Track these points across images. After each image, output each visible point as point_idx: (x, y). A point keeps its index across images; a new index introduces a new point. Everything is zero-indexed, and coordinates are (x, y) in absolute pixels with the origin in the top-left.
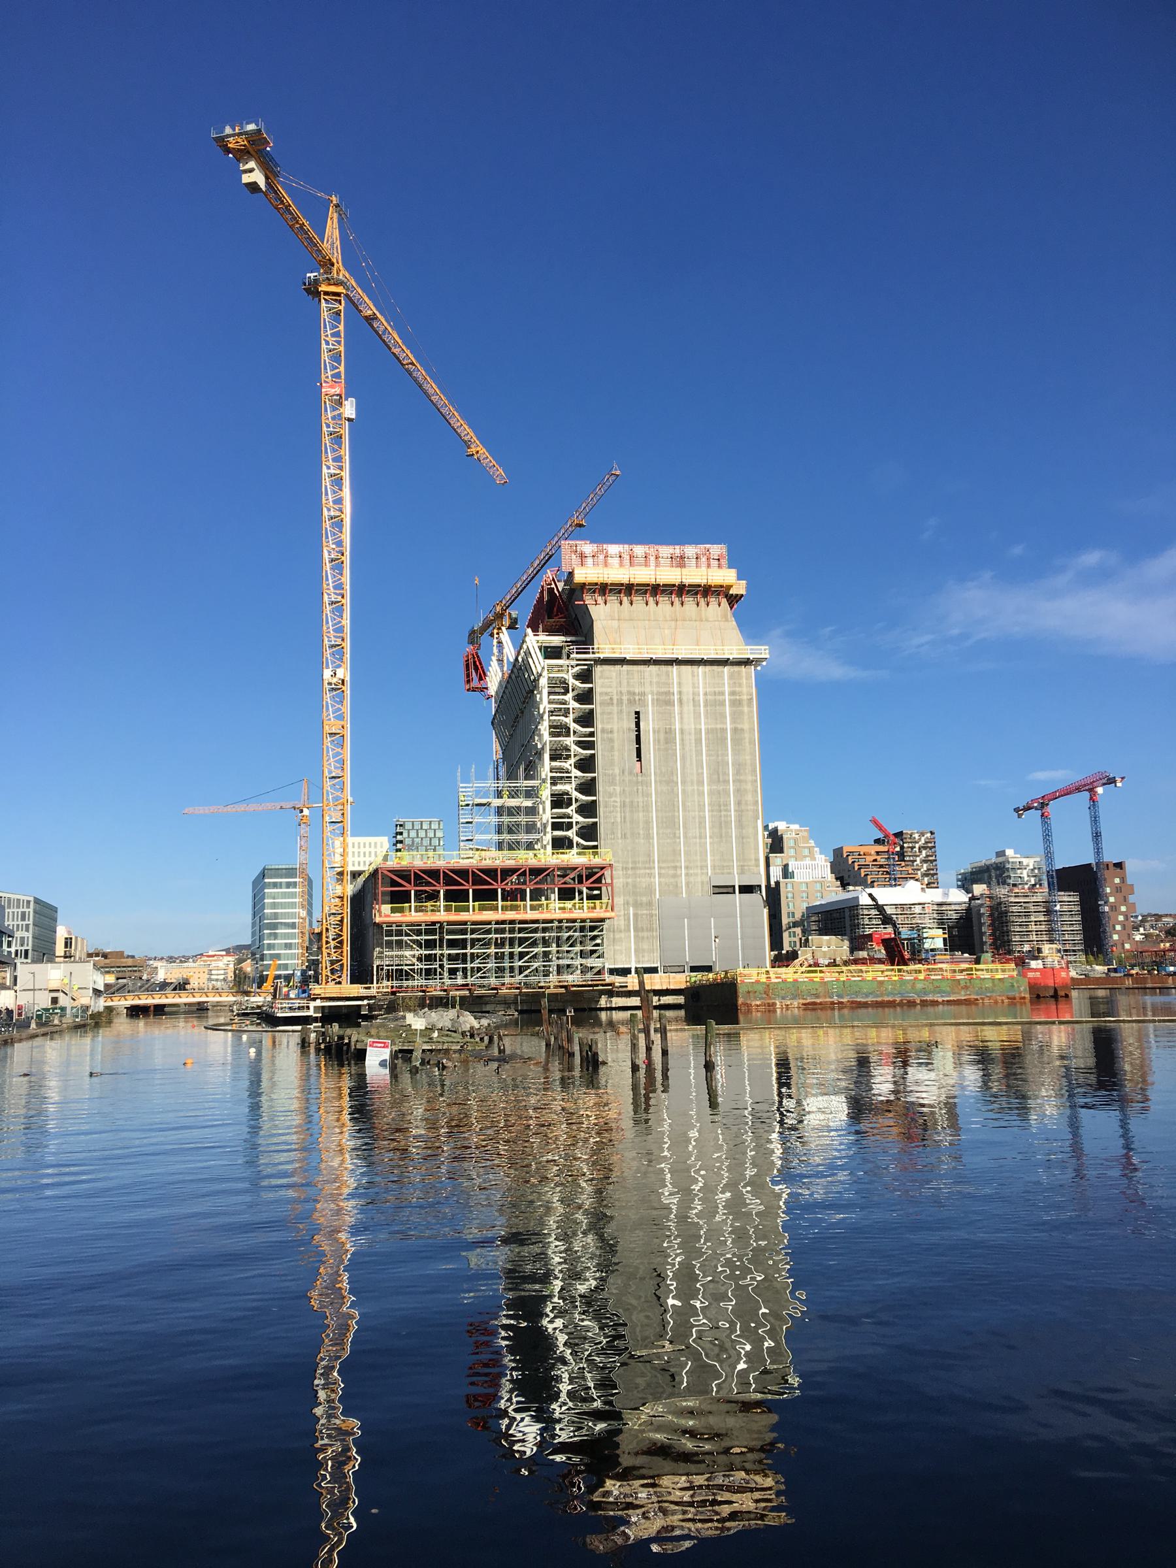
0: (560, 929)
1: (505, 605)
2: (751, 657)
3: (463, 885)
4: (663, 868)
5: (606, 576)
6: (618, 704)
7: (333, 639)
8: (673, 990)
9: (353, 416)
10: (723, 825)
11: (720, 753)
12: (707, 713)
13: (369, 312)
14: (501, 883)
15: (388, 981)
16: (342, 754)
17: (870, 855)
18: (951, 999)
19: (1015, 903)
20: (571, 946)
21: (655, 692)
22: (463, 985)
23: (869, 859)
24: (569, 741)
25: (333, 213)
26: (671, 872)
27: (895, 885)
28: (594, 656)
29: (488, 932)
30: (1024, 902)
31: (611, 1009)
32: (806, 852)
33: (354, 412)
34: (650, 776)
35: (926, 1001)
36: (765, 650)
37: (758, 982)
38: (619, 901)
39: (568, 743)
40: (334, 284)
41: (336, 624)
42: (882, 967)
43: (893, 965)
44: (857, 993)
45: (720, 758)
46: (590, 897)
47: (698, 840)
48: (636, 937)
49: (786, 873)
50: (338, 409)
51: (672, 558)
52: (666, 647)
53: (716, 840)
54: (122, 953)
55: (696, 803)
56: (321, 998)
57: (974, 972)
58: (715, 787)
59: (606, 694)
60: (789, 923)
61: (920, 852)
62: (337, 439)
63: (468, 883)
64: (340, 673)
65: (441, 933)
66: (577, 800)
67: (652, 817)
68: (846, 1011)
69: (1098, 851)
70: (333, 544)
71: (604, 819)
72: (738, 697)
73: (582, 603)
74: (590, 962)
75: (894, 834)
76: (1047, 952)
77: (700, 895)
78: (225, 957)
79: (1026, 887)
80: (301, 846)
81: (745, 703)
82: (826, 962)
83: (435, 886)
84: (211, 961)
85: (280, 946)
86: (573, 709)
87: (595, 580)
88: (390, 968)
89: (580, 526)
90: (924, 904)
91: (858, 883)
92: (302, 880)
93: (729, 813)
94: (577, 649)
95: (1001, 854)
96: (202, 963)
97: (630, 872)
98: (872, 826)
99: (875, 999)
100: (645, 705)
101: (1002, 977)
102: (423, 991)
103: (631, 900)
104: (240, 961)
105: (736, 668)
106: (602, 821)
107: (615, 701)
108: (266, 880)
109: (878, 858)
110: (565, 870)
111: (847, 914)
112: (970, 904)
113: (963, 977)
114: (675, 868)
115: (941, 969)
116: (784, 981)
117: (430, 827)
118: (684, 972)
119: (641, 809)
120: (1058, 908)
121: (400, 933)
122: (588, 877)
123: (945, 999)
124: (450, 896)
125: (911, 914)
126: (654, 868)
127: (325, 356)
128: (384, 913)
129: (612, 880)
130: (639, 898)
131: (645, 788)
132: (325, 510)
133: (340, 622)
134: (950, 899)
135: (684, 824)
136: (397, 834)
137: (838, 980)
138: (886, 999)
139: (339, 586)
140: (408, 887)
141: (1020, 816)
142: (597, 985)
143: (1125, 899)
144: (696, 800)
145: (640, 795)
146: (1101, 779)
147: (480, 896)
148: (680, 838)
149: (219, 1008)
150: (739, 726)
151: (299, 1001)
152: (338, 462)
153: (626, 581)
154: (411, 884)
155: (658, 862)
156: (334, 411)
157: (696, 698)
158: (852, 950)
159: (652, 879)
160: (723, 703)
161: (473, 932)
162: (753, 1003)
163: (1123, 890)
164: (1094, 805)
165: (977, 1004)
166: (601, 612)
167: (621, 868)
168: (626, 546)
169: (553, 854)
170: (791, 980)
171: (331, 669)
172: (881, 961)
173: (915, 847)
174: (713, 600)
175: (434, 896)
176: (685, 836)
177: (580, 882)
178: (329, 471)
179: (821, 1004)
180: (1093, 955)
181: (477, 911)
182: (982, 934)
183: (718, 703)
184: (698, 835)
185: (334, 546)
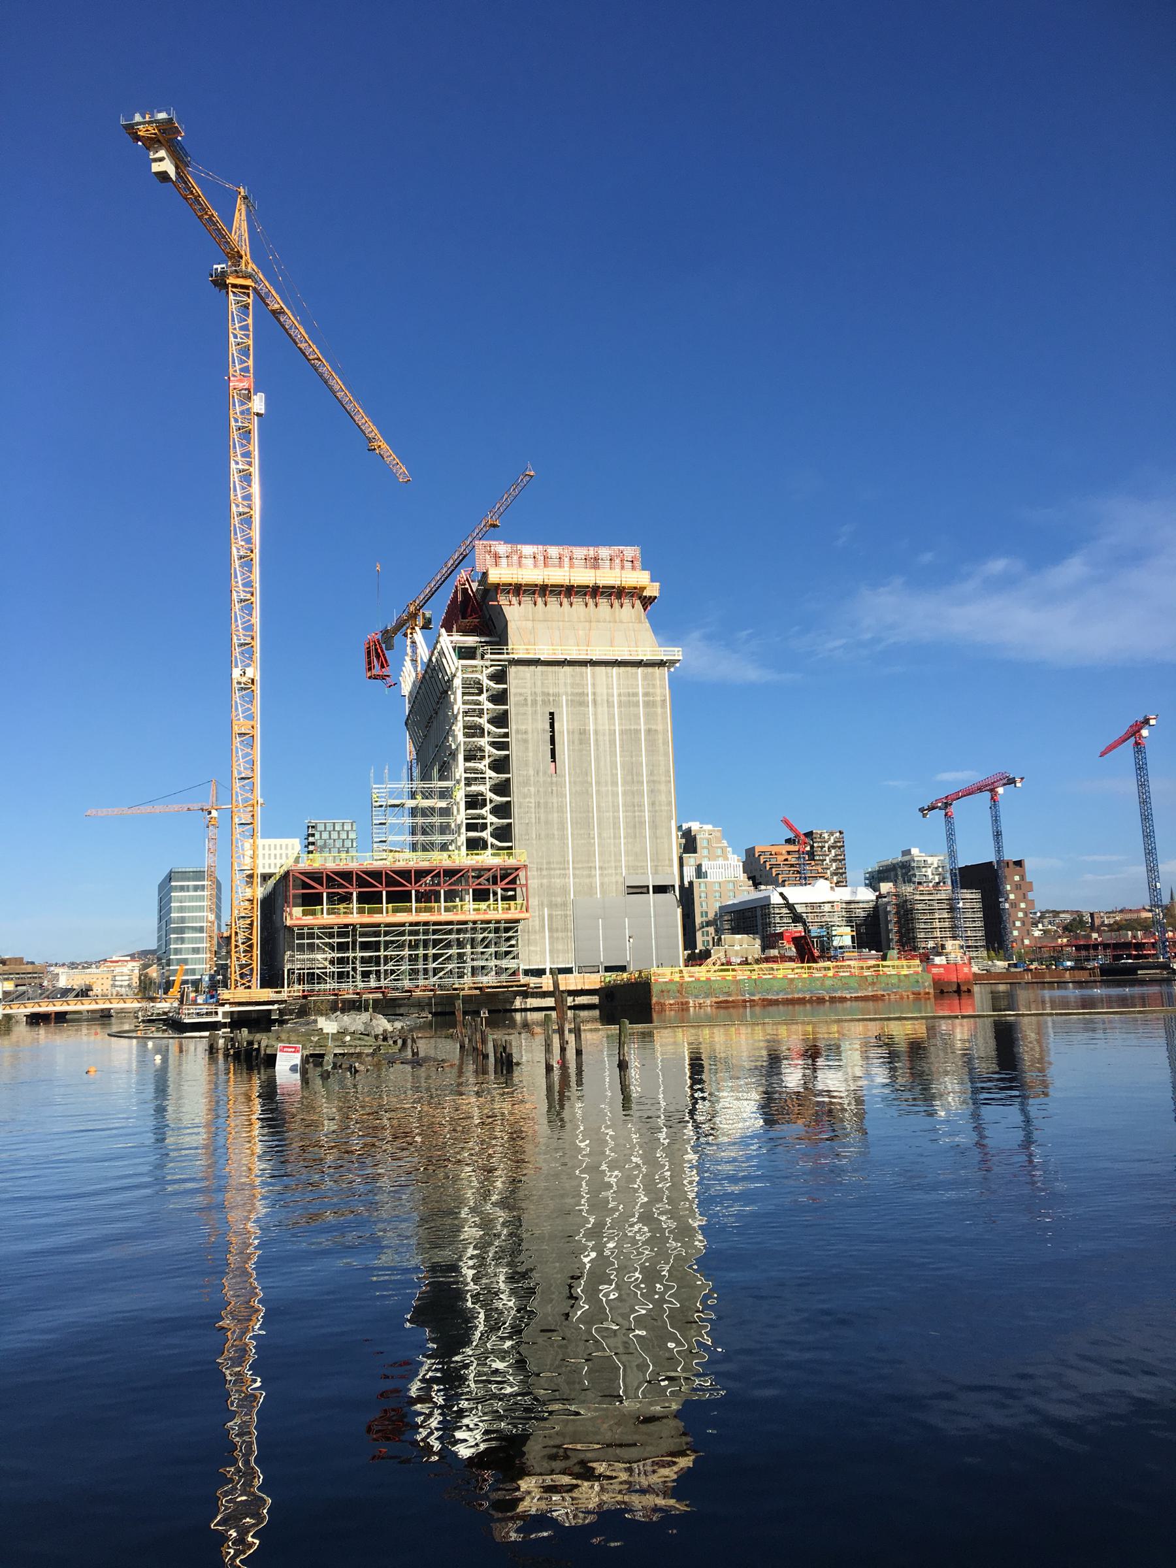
0: (474, 930)
1: (418, 605)
2: (665, 658)
3: (377, 887)
4: (579, 869)
5: (520, 576)
6: (532, 704)
7: (242, 637)
9: (262, 411)
10: (637, 826)
11: (634, 753)
13: (277, 306)
14: (415, 884)
15: (300, 984)
17: (781, 854)
18: (859, 995)
20: (486, 947)
21: (569, 693)
22: (377, 988)
23: (781, 858)
24: (483, 742)
27: (806, 884)
29: (402, 934)
30: (929, 900)
31: (526, 1010)
32: (719, 852)
33: (263, 407)
34: (565, 777)
35: (835, 997)
36: (678, 651)
37: (671, 981)
38: (534, 902)
39: (483, 745)
40: (243, 277)
41: (245, 622)
43: (803, 962)
44: (768, 991)
46: (504, 898)
47: (612, 841)
48: (550, 938)
49: (699, 873)
51: (586, 559)
54: (22, 959)
55: (611, 804)
56: (230, 1003)
57: (881, 969)
59: (521, 694)
60: (702, 922)
61: (830, 851)
62: (246, 434)
63: (352, 885)
64: (250, 672)
65: (354, 935)
66: (491, 801)
67: (567, 818)
68: (757, 1009)
69: (999, 850)
70: (242, 540)
71: (518, 821)
72: (651, 699)
75: (804, 834)
76: (950, 948)
77: (614, 895)
78: (129, 963)
79: (931, 885)
80: (209, 849)
81: (659, 704)
83: (348, 888)
84: (115, 967)
85: (188, 951)
86: (487, 709)
87: (509, 580)
89: (495, 526)
90: (833, 902)
94: (491, 649)
95: (907, 852)
96: (105, 969)
97: (545, 873)
99: (785, 997)
100: (559, 706)
101: (907, 973)
104: (146, 966)
105: (650, 670)
106: (516, 821)
107: (529, 702)
108: (173, 884)
109: (789, 857)
110: (480, 872)
111: (759, 913)
112: (877, 902)
113: (870, 974)
115: (849, 966)
116: (698, 980)
118: (599, 972)
119: (555, 809)
120: (961, 905)
121: (311, 936)
122: (503, 878)
123: (853, 995)
125: (820, 913)
126: (569, 869)
127: (233, 350)
128: (295, 916)
131: (559, 789)
132: (233, 506)
133: (250, 620)
134: (859, 898)
135: (599, 824)
136: (309, 835)
137: (749, 978)
138: (796, 996)
140: (320, 889)
141: (924, 816)
142: (512, 986)
143: (1025, 896)
145: (555, 795)
147: (393, 898)
148: (594, 838)
149: (123, 1015)
150: (654, 727)
151: (206, 1007)
155: (573, 862)
157: (611, 700)
159: (567, 880)
160: (637, 704)
161: (386, 934)
162: (667, 1002)
163: (1023, 888)
166: (515, 613)
169: (467, 855)
171: (240, 668)
172: (791, 959)
173: (824, 847)
175: (346, 898)
177: (495, 883)
179: (733, 1002)
180: (994, 950)
181: (390, 913)
182: (888, 931)
184: (612, 835)
185: (243, 543)
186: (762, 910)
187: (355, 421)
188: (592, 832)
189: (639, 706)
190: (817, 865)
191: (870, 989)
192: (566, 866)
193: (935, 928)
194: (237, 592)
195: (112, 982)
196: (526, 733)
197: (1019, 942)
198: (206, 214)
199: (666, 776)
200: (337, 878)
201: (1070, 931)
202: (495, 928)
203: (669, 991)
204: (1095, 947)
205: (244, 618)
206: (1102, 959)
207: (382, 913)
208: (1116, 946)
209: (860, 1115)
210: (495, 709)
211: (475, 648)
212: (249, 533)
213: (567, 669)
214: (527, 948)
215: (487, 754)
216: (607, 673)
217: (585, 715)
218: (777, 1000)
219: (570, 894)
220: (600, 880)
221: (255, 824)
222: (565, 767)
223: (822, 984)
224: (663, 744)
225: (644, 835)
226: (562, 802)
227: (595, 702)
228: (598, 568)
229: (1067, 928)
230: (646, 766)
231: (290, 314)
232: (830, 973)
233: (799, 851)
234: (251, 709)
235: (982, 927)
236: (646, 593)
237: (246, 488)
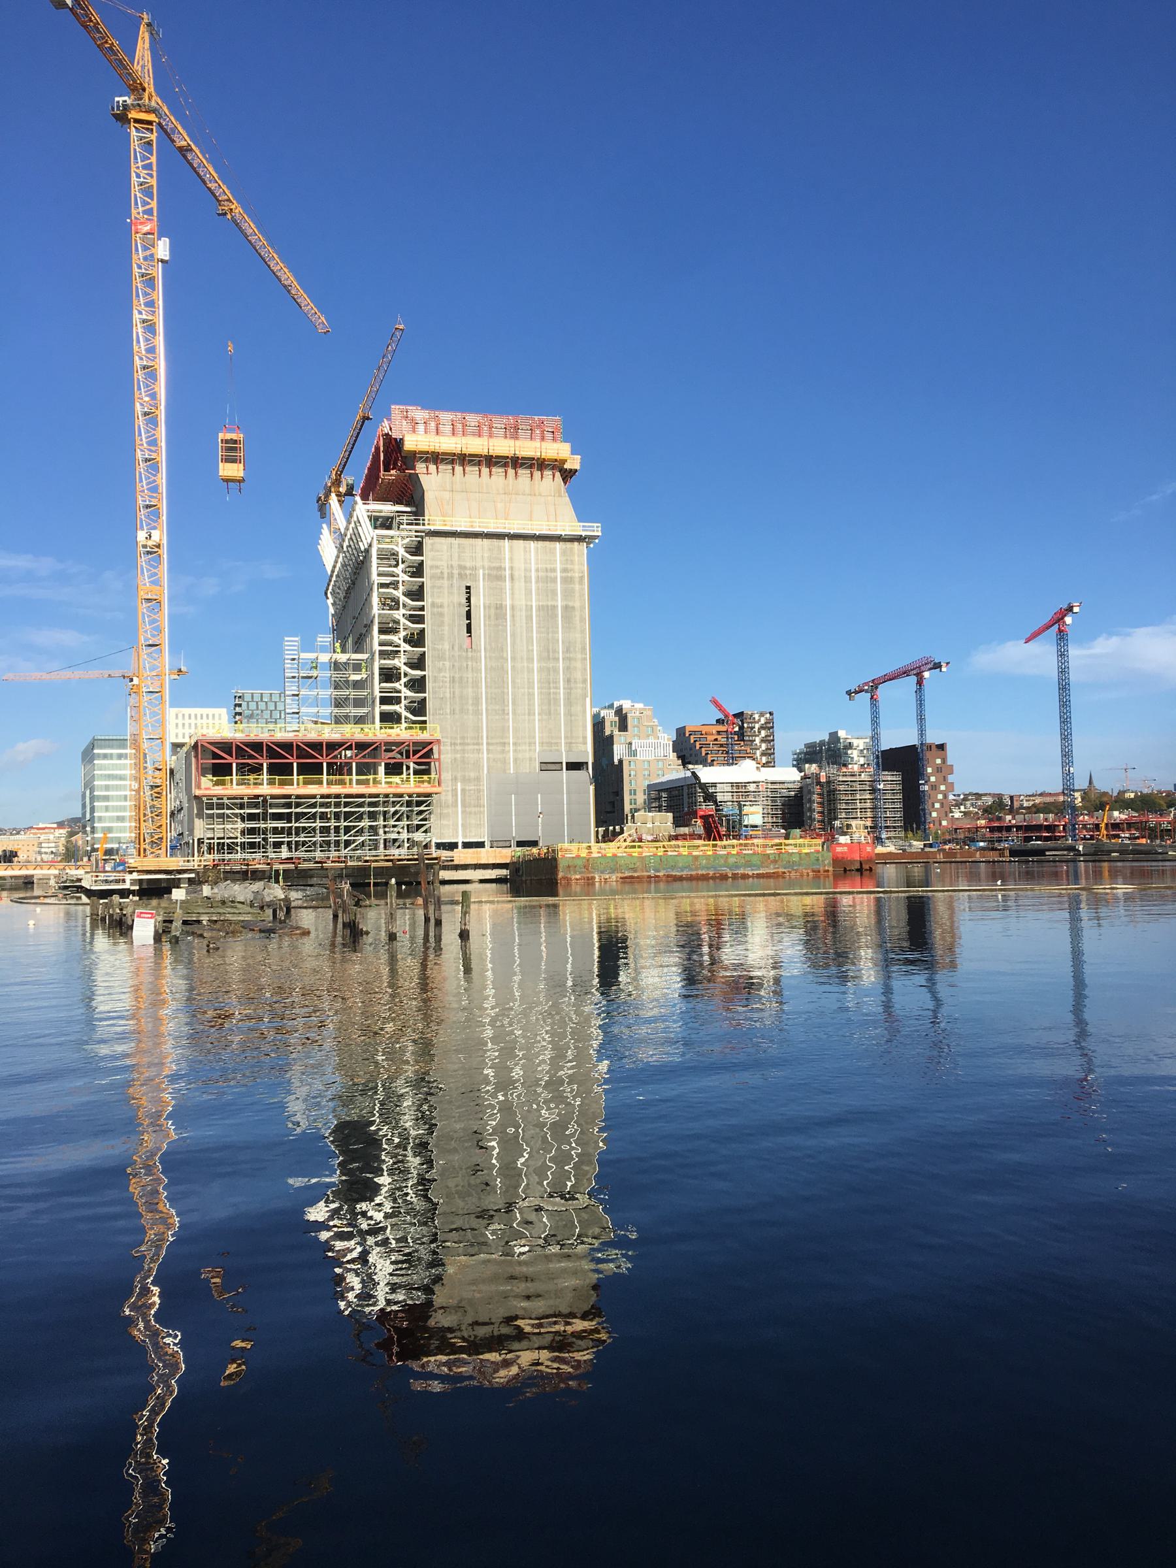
2: (584, 534)
3: (288, 758)
4: (492, 744)
5: (437, 445)
6: (448, 579)
8: (480, 864)
9: (167, 258)
10: (552, 702)
11: (550, 630)
12: (538, 589)
13: (183, 143)
14: (327, 756)
15: (210, 854)
18: (761, 872)
20: (398, 820)
22: (287, 859)
23: (711, 738)
24: (399, 614)
25: (143, 33)
26: (499, 748)
27: (732, 764)
28: (424, 527)
30: (851, 781)
33: (168, 253)
34: (480, 652)
36: (597, 527)
37: (578, 856)
38: (446, 776)
39: (397, 617)
40: (146, 112)
42: (701, 842)
44: (673, 868)
45: (550, 635)
46: (416, 772)
47: (527, 717)
48: (462, 812)
50: (150, 249)
51: (505, 428)
52: (446, 519)
53: (545, 717)
55: (526, 680)
56: (138, 871)
57: (783, 847)
58: (545, 665)
59: (437, 567)
61: (759, 732)
62: (150, 282)
63: (293, 757)
64: (156, 535)
66: (406, 675)
67: (482, 693)
68: (662, 885)
70: (146, 396)
72: (569, 575)
73: (413, 472)
74: (418, 836)
75: (733, 715)
78: (56, 830)
81: (577, 580)
82: (650, 838)
83: (257, 759)
84: (41, 834)
85: (111, 819)
86: (403, 582)
88: (212, 841)
91: (699, 762)
92: (134, 751)
96: (32, 835)
97: (458, 748)
98: (713, 707)
100: (476, 579)
102: (248, 865)
104: (72, 834)
105: (569, 545)
109: (719, 737)
110: (390, 746)
113: (773, 852)
114: (504, 744)
116: (604, 856)
118: (510, 846)
119: (470, 685)
120: (881, 787)
121: (221, 806)
122: (415, 752)
123: (755, 872)
124: (273, 770)
125: (745, 792)
126: (482, 744)
127: (135, 190)
129: (439, 755)
130: (467, 774)
132: (136, 358)
137: (655, 855)
138: (700, 872)
140: (229, 760)
143: (945, 779)
144: (526, 677)
146: (926, 664)
147: (242, 769)
148: (508, 714)
150: (571, 604)
151: (114, 874)
153: (511, 454)
155: (487, 738)
158: (677, 823)
159: (480, 755)
160: (554, 580)
162: (573, 877)
163: (944, 771)
166: (431, 480)
167: (449, 744)
168: (459, 415)
169: (381, 728)
170: (610, 855)
172: (700, 837)
174: (548, 473)
175: (257, 769)
176: (514, 713)
177: (408, 757)
178: (141, 316)
180: (912, 831)
182: (811, 810)
183: (549, 579)
184: (527, 712)
185: (147, 399)
186: (688, 789)
188: (506, 708)
191: (772, 866)
192: (480, 741)
194: (142, 450)
195: (38, 849)
197: (937, 823)
199: (582, 653)
202: (407, 801)
203: (575, 867)
204: (1009, 829)
206: (1014, 840)
207: (293, 785)
208: (1029, 828)
210: (412, 582)
211: (392, 518)
212: (154, 389)
215: (402, 627)
216: (525, 548)
217: (502, 589)
218: (681, 876)
219: (483, 770)
222: (480, 641)
223: (726, 861)
224: (580, 622)
227: (512, 577)
229: (987, 810)
234: (157, 574)
235: (900, 808)
236: (567, 466)
237: (150, 340)
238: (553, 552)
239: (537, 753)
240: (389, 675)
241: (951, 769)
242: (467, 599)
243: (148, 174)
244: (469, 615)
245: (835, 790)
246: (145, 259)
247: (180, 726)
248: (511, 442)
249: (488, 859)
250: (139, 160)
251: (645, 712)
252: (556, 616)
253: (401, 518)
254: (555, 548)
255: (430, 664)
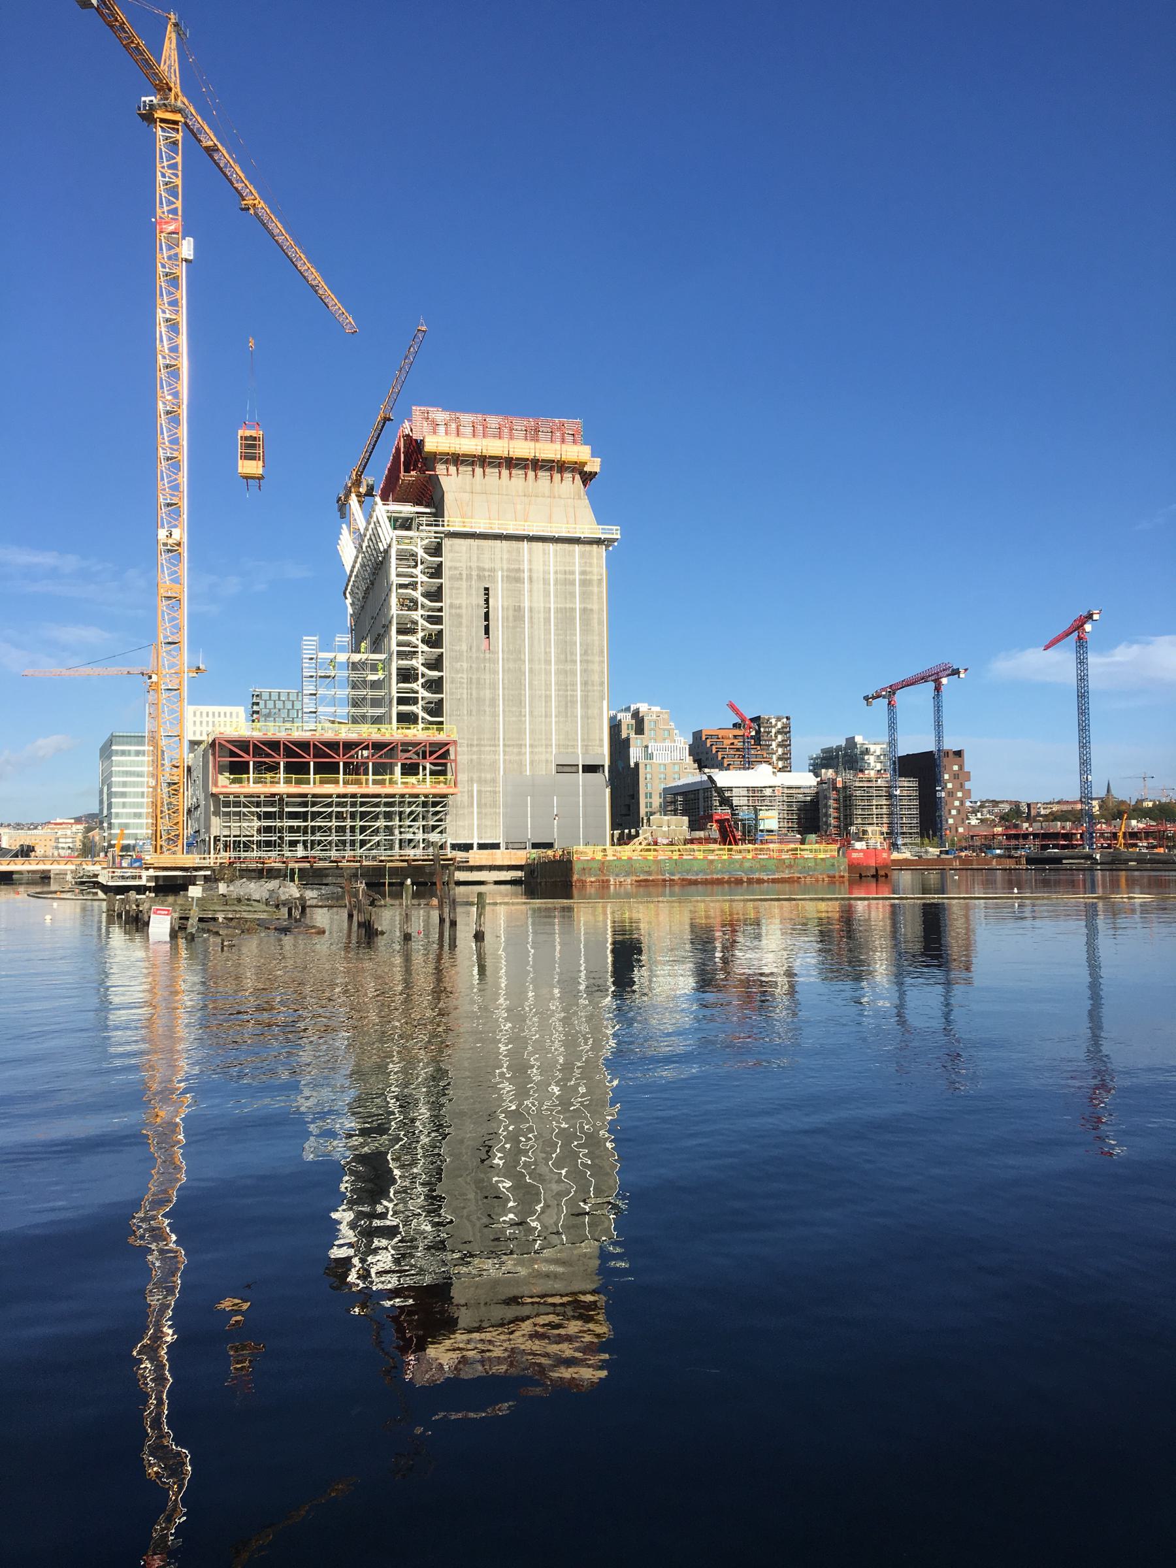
2: (603, 536)
4: (509, 746)
6: (467, 580)
7: (169, 496)
8: (513, 866)
9: (191, 258)
10: (569, 704)
11: (568, 632)
13: (210, 143)
15: (226, 851)
16: (178, 619)
17: (729, 738)
18: (776, 877)
19: (859, 787)
20: (413, 820)
21: (505, 568)
22: (303, 858)
24: (417, 615)
25: (170, 33)
26: (515, 750)
27: (748, 768)
30: (867, 787)
33: (192, 253)
36: (617, 530)
37: (593, 859)
38: (463, 777)
40: (172, 112)
43: (725, 844)
44: (688, 872)
46: (432, 773)
47: (544, 719)
48: (479, 813)
51: (526, 430)
55: (543, 682)
56: (154, 868)
57: (799, 852)
59: (456, 568)
61: (776, 737)
62: (174, 281)
64: (177, 534)
66: (423, 675)
67: (499, 695)
68: (677, 889)
70: (169, 394)
72: (588, 577)
74: (434, 837)
75: (750, 719)
81: (595, 583)
82: (665, 841)
84: (59, 829)
85: (128, 815)
87: (446, 450)
90: (775, 787)
92: (151, 748)
93: (575, 693)
96: (49, 831)
98: (730, 711)
100: (494, 581)
101: (824, 856)
103: (475, 776)
104: (89, 830)
105: (588, 547)
107: (464, 576)
108: (114, 748)
109: (736, 741)
110: (406, 746)
113: (788, 857)
115: (768, 849)
117: (289, 698)
118: (526, 848)
119: (487, 686)
120: (898, 793)
121: (237, 804)
122: (432, 753)
123: (770, 877)
125: (761, 797)
126: (499, 745)
127: (161, 190)
129: (456, 757)
130: (483, 775)
132: (159, 357)
133: (176, 480)
136: (253, 704)
138: (715, 876)
139: (175, 441)
140: (246, 758)
143: (962, 786)
147: (321, 769)
148: (525, 716)
150: (589, 606)
151: (131, 870)
152: (174, 306)
154: (249, 755)
155: (504, 739)
156: (170, 250)
158: (693, 827)
159: (497, 757)
160: (573, 583)
162: (588, 880)
163: (961, 777)
164: (938, 695)
165: (799, 882)
166: (451, 481)
167: (465, 745)
168: (480, 417)
169: (398, 728)
171: (166, 529)
172: (715, 841)
174: (568, 476)
175: (274, 768)
177: (424, 757)
179: (653, 881)
180: (929, 838)
182: (827, 815)
185: (169, 398)
186: (704, 793)
187: (296, 266)
188: (523, 710)
189: (575, 585)
190: (764, 749)
191: (787, 872)
192: (497, 742)
193: (872, 815)
195: (55, 844)
196: (460, 607)
198: (132, 42)
199: (599, 656)
200: (263, 747)
201: (1007, 821)
202: (423, 802)
204: (1026, 836)
205: (170, 477)
206: (1031, 848)
207: (309, 784)
208: (1046, 836)
209: (792, 991)
210: (431, 583)
212: (176, 387)
213: (506, 544)
214: (454, 823)
215: (420, 628)
216: (544, 550)
217: (520, 591)
220: (530, 758)
221: (182, 690)
225: (575, 714)
226: (494, 679)
227: (531, 579)
228: (537, 440)
229: (1004, 818)
230: (580, 645)
231: (224, 152)
232: (750, 856)
233: (743, 736)
235: (916, 814)
237: (173, 339)
238: (572, 554)
239: (553, 755)
240: (406, 675)
241: (968, 776)
242: (485, 600)
243: (173, 174)
244: (487, 617)
245: (851, 796)
246: (170, 258)
247: (198, 723)
248: (532, 444)
249: (503, 860)
250: (165, 160)
251: (661, 716)
252: (575, 618)
253: (421, 519)
254: (574, 551)
255: (448, 664)
